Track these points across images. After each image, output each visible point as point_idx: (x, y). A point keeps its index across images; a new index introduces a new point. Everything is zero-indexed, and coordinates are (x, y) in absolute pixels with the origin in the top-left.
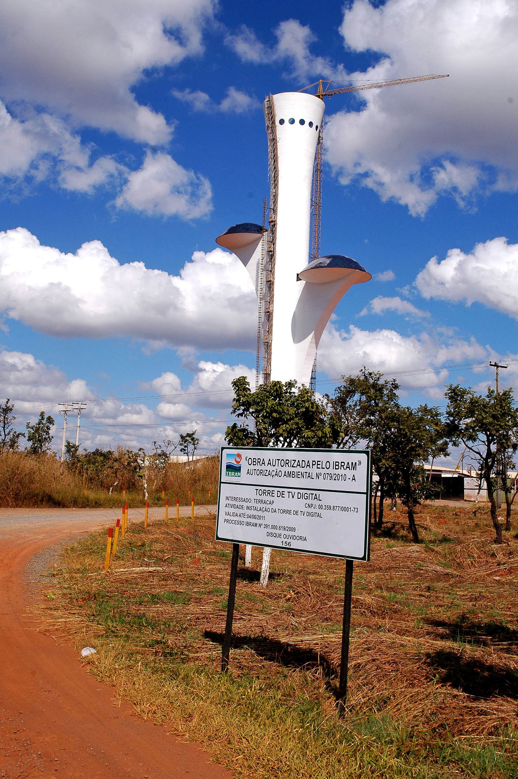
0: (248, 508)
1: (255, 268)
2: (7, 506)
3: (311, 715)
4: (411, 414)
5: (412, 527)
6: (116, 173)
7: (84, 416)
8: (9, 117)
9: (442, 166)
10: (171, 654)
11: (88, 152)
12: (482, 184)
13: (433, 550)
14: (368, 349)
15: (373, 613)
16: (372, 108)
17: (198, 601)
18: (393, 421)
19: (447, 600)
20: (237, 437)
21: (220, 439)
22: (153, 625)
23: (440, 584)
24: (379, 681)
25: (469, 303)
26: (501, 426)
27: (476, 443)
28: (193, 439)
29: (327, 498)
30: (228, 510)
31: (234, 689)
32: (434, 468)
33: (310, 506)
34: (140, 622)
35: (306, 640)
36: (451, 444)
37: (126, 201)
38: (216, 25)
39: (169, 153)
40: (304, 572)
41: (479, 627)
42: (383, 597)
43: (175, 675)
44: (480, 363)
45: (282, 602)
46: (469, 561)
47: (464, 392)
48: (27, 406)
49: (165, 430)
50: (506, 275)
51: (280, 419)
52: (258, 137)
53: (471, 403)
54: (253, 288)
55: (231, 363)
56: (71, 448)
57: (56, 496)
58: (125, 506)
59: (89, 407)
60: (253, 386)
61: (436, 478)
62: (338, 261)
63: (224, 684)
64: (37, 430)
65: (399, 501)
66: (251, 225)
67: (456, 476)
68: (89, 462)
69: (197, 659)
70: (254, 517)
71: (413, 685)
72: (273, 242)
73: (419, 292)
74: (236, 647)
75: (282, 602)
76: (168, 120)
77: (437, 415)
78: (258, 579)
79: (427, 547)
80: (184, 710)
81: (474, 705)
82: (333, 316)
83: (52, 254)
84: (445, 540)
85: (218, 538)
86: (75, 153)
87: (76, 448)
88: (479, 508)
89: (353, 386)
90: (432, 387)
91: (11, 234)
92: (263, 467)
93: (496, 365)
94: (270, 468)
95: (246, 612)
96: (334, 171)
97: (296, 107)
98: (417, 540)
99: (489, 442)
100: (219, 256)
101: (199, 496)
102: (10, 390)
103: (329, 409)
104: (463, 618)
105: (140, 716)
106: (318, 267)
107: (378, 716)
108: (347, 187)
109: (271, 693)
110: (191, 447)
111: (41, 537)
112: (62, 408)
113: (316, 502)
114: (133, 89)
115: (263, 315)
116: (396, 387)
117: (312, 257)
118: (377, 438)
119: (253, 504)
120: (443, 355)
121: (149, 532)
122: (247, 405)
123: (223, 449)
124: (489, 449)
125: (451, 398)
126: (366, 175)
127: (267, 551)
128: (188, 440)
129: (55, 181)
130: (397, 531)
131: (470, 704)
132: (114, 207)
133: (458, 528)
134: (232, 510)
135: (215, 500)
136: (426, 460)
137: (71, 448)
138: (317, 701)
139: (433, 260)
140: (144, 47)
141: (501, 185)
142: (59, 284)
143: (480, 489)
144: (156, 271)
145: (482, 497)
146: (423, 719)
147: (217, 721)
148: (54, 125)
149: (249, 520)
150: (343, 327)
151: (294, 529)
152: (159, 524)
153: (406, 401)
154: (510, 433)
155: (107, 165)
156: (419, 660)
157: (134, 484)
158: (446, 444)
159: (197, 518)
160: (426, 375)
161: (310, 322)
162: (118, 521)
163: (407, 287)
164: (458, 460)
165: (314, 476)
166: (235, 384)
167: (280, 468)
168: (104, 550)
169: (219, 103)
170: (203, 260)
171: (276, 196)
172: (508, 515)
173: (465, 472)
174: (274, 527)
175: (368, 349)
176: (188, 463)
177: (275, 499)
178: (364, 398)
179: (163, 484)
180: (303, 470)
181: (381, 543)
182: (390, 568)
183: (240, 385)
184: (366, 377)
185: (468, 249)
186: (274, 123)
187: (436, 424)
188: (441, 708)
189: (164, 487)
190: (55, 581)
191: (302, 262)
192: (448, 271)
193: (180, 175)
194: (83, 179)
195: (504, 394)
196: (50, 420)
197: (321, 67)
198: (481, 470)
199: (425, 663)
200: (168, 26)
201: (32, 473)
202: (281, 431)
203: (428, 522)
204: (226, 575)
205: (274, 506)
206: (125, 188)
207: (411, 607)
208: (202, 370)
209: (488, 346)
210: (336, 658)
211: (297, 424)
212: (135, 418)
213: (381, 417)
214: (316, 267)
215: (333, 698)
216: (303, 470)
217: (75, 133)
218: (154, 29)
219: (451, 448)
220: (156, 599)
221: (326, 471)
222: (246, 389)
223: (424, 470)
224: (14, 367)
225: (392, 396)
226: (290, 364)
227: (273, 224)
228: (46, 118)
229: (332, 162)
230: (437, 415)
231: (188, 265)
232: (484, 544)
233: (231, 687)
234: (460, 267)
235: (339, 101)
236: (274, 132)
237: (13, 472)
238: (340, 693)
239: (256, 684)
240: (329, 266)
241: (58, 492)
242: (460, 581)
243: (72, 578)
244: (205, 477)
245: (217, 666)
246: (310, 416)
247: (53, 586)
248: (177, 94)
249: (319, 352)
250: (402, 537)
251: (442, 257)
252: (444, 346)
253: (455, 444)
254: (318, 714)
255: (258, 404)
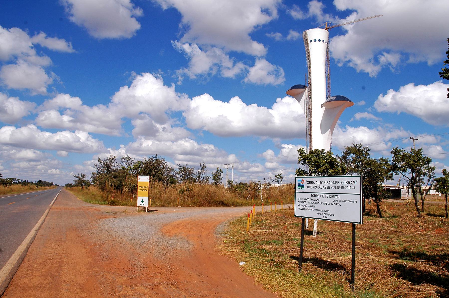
0: (308, 202)
1: (303, 103)
2: (206, 206)
3: (339, 290)
4: (376, 161)
5: (379, 211)
6: (244, 69)
7: (234, 169)
8: (200, 51)
9: (382, 55)
10: (277, 265)
11: (232, 61)
12: (402, 61)
13: (389, 221)
14: (355, 135)
15: (364, 248)
16: (350, 32)
17: (287, 243)
18: (368, 165)
19: (397, 242)
20: (300, 173)
21: (293, 176)
22: (269, 253)
23: (393, 236)
24: (369, 276)
25: (399, 113)
26: (418, 165)
27: (406, 173)
28: (280, 177)
29: (342, 197)
30: (299, 204)
31: (305, 279)
32: (387, 185)
33: (335, 201)
34: (263, 252)
35: (335, 259)
36: (394, 174)
37: (249, 80)
38: (284, 6)
39: (265, 58)
40: (331, 231)
41: (413, 253)
42: (368, 241)
43: (279, 273)
44: (406, 138)
45: (323, 244)
46: (406, 225)
47: (400, 151)
48: (211, 166)
49: (268, 174)
50: (415, 99)
51: (319, 165)
52: (301, 50)
53: (403, 155)
54: (303, 112)
55: (296, 144)
56: (230, 182)
57: (225, 202)
58: (254, 205)
59: (237, 165)
60: (307, 152)
61: (388, 190)
62: (339, 98)
63: (301, 277)
64: (216, 175)
65: (372, 200)
66: (300, 85)
67: (397, 189)
68: (238, 187)
69: (288, 267)
70: (311, 206)
71: (384, 278)
72: (310, 91)
73: (376, 110)
74: (304, 262)
75: (323, 244)
76: (265, 46)
77: (388, 161)
78: (312, 234)
79: (386, 219)
80: (284, 287)
81: (414, 287)
82: (339, 122)
83: (219, 103)
84: (394, 216)
85: (295, 216)
86: (227, 62)
87: (232, 182)
88: (409, 202)
89: (349, 150)
90: (384, 150)
91: (202, 96)
92: (314, 185)
93: (413, 139)
94: (317, 185)
95: (308, 248)
96: (336, 60)
97: (317, 35)
98: (381, 217)
99: (412, 172)
100: (288, 99)
101: (284, 200)
102: (205, 159)
103: (339, 160)
104: (405, 249)
105: (265, 289)
106: (331, 101)
107: (369, 291)
108: (342, 67)
109: (321, 281)
110: (280, 180)
111: (220, 218)
112: (226, 166)
113: (338, 199)
114: (250, 35)
115: (308, 123)
116: (369, 150)
117: (327, 97)
118: (361, 172)
119: (310, 201)
120: (389, 136)
121: (264, 216)
122: (304, 160)
123: (296, 178)
124: (413, 176)
125: (394, 153)
126: (349, 61)
127: (316, 221)
128: (279, 177)
129: (220, 74)
130: (372, 213)
131: (412, 287)
132: (244, 82)
133: (399, 211)
134: (301, 204)
135: (293, 201)
136: (383, 182)
137: (230, 182)
138: (341, 284)
139: (381, 95)
140: (254, 18)
141: (412, 60)
142: (222, 115)
143: (408, 194)
144: (262, 107)
145: (409, 198)
146: (390, 293)
147: (299, 292)
148: (218, 52)
149: (309, 208)
150: (343, 127)
151: (329, 211)
152: (268, 212)
153: (373, 156)
154: (422, 168)
155: (240, 66)
156: (386, 267)
157: (257, 196)
158: (392, 174)
159: (284, 210)
160: (381, 145)
161: (328, 125)
162: (252, 211)
163: (370, 108)
164: (398, 181)
165: (337, 188)
166: (299, 151)
167: (321, 185)
168: (246, 223)
169: (286, 37)
170: (281, 101)
171: (310, 73)
172: (423, 205)
173: (401, 187)
174: (320, 210)
175: (355, 135)
176: (279, 187)
177: (320, 198)
178: (354, 156)
179: (269, 196)
180: (331, 185)
181: (366, 218)
182: (370, 229)
183: (301, 151)
184: (355, 147)
185: (397, 89)
186: (307, 42)
187: (388, 165)
188: (398, 288)
189: (269, 197)
190: (227, 236)
191: (323, 100)
192: (388, 99)
193: (269, 67)
194: (231, 72)
195: (418, 151)
196: (221, 171)
197: (328, 18)
198: (408, 186)
199: (389, 269)
200: (263, 9)
201: (215, 193)
202: (320, 170)
203: (385, 209)
204: (298, 232)
205: (319, 201)
206: (248, 74)
207: (381, 245)
208: (283, 148)
209: (408, 131)
210: (349, 267)
211: (326, 167)
212: (256, 169)
213: (362, 164)
214: (330, 101)
215: (348, 283)
216: (331, 185)
217: (227, 54)
218: (258, 10)
219: (394, 176)
220: (269, 243)
221: (342, 185)
222: (303, 153)
223: (382, 187)
224: (206, 150)
225: (367, 154)
226: (320, 142)
227: (310, 84)
228: (215, 48)
229: (334, 58)
230: (388, 161)
231: (275, 104)
232: (412, 218)
233: (304, 278)
234: (394, 98)
235: (335, 31)
236: (308, 46)
237: (208, 193)
238: (352, 281)
239: (314, 277)
240: (335, 100)
241: (226, 200)
242: (402, 234)
243: (233, 234)
244: (287, 192)
245: (297, 270)
246: (332, 164)
247: (226, 238)
248: (267, 35)
249: (333, 138)
250: (374, 215)
251: (385, 93)
252: (389, 132)
253: (396, 174)
254: (342, 290)
255: (309, 159)
